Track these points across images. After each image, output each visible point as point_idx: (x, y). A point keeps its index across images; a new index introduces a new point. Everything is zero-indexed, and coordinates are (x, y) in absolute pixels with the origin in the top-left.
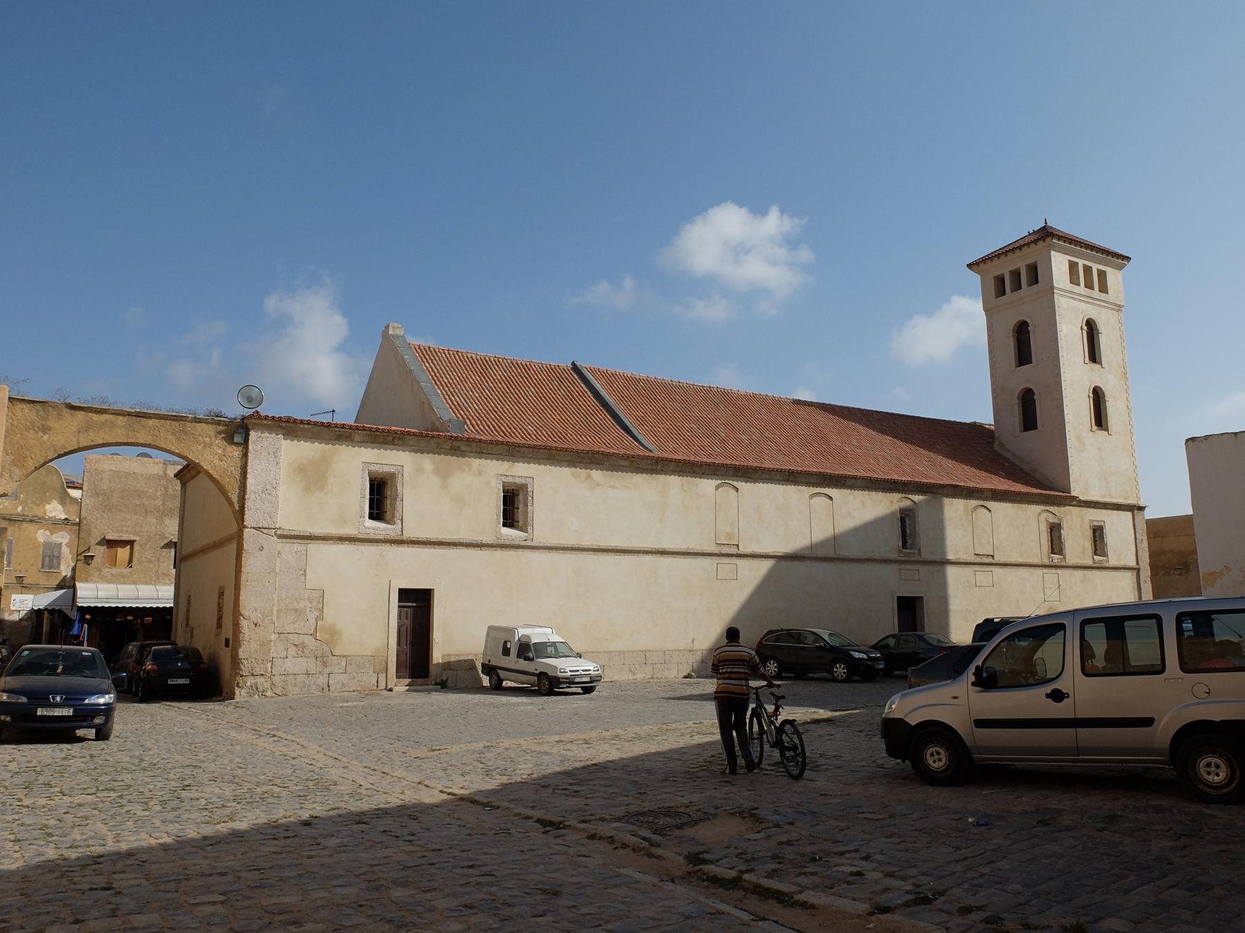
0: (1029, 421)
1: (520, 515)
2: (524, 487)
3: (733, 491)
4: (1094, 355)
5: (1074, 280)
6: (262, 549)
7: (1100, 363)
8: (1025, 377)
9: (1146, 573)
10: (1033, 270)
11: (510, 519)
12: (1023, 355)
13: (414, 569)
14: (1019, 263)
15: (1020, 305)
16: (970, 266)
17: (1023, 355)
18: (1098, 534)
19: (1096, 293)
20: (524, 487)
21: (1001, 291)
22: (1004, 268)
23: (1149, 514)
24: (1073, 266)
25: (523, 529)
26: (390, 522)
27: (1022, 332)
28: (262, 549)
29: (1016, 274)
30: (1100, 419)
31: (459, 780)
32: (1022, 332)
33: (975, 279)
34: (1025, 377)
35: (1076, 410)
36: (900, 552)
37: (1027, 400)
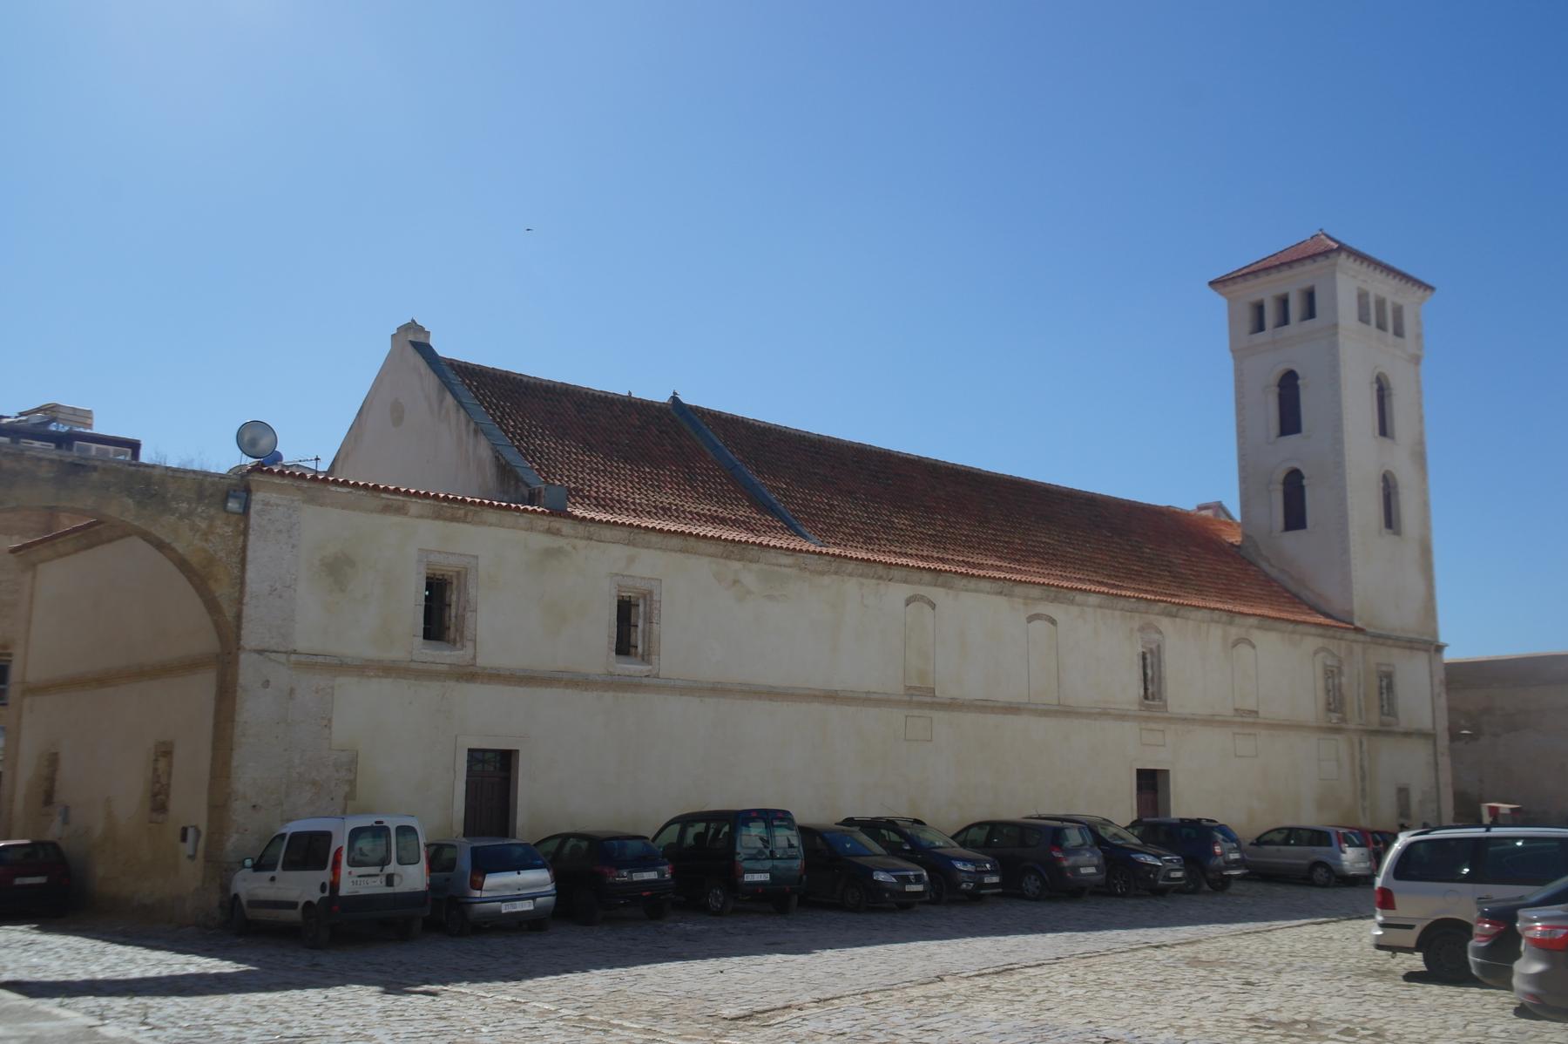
0: (1295, 517)
1: (638, 637)
2: (647, 596)
3: (927, 609)
4: (1384, 429)
5: (1363, 318)
6: (266, 684)
7: (1392, 438)
8: (1290, 453)
9: (1444, 741)
10: (1310, 297)
11: (624, 647)
12: (1290, 421)
13: (488, 717)
14: (1291, 284)
15: (1292, 347)
16: (1211, 283)
17: (1290, 421)
18: (1387, 684)
19: (1390, 334)
20: (647, 596)
21: (1259, 326)
22: (1266, 290)
23: (1449, 656)
24: (1362, 297)
25: (646, 658)
26: (649, 663)
27: (1289, 385)
28: (266, 684)
29: (1283, 302)
30: (1391, 519)
31: (56, 965)
32: (1289, 385)
33: (1219, 304)
34: (1290, 453)
35: (1364, 507)
36: (1141, 704)
37: (1294, 486)
